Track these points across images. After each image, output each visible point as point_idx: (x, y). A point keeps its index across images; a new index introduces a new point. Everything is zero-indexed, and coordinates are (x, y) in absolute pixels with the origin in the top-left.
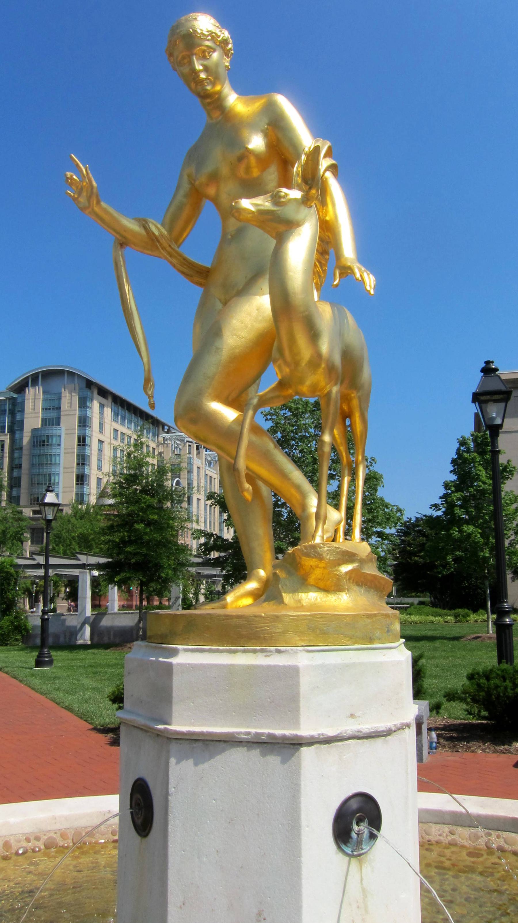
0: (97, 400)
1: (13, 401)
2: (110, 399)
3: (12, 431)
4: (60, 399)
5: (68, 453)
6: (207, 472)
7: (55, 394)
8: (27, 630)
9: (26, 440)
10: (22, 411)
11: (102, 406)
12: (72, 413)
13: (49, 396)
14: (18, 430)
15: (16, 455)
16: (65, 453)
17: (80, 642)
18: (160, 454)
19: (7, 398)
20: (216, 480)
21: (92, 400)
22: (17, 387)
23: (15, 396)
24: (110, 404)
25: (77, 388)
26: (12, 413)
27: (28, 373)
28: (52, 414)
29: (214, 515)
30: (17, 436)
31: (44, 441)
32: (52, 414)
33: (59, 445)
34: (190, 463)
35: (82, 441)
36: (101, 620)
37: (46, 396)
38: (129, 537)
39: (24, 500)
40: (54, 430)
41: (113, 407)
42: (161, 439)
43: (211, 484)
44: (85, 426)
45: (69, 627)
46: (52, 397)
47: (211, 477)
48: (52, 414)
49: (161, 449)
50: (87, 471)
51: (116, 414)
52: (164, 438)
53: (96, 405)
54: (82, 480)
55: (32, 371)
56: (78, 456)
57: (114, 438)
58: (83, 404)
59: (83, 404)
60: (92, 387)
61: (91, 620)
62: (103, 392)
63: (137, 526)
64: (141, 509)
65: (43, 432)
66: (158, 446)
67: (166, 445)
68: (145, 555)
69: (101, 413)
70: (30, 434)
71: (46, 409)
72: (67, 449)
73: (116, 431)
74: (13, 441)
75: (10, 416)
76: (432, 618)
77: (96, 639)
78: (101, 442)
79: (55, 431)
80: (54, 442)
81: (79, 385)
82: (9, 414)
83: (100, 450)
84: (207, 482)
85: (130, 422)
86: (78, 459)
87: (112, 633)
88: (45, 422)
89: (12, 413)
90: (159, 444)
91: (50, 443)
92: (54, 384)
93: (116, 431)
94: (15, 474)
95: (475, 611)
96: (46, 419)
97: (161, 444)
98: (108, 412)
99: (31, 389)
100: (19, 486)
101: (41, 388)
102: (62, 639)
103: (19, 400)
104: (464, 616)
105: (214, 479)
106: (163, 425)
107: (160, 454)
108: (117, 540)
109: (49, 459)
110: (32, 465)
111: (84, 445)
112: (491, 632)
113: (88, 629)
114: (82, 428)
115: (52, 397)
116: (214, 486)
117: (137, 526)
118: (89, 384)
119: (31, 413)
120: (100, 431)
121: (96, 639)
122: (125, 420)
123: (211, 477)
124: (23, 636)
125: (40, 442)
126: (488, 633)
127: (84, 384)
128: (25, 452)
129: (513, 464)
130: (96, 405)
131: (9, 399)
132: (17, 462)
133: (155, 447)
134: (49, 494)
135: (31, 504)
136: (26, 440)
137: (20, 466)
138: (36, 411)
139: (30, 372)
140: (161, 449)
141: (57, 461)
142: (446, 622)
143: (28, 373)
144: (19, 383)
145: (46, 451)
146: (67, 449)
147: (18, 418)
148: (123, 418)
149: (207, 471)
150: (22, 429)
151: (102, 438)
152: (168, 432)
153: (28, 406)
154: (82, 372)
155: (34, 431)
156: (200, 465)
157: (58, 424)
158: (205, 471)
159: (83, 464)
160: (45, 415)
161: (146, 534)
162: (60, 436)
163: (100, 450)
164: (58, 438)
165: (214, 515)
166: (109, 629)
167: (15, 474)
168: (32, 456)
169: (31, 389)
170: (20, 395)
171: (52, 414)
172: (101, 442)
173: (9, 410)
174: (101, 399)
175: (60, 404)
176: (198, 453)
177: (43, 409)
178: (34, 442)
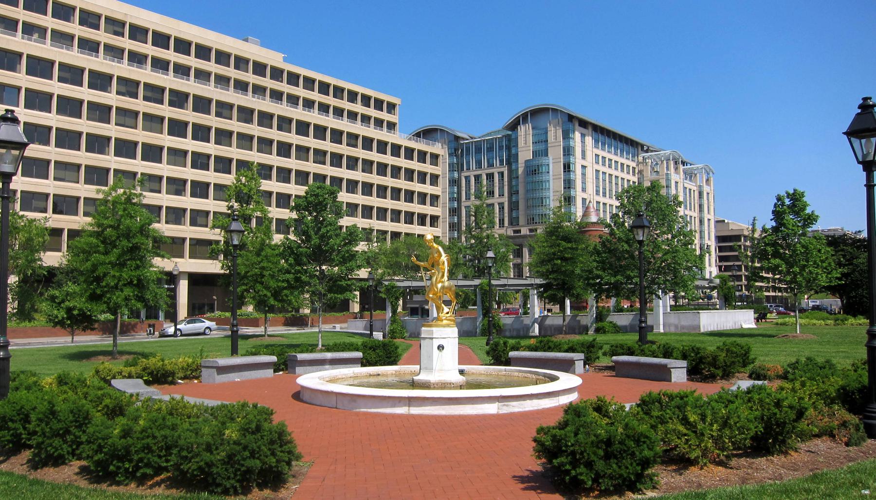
0: (579, 131)
1: (508, 137)
2: (590, 129)
3: (509, 163)
4: (547, 133)
5: (556, 179)
6: (686, 185)
7: (543, 129)
8: (499, 326)
9: (521, 170)
10: (517, 146)
11: (583, 136)
12: (557, 144)
13: (538, 131)
14: (514, 162)
15: (514, 183)
16: (553, 179)
17: (531, 334)
18: (640, 172)
19: (503, 136)
20: (696, 192)
21: (574, 132)
22: (512, 125)
23: (510, 133)
24: (591, 132)
25: (560, 123)
26: (509, 148)
27: (519, 113)
28: (541, 147)
29: (695, 224)
30: (514, 167)
31: (535, 171)
32: (541, 147)
33: (548, 172)
34: (668, 180)
35: (567, 168)
36: (546, 320)
37: (535, 132)
38: (552, 268)
39: (522, 221)
40: (543, 160)
41: (594, 135)
42: (641, 159)
43: (690, 196)
44: (569, 155)
45: (525, 325)
46: (540, 132)
47: (690, 190)
48: (541, 147)
49: (641, 167)
50: (572, 193)
51: (596, 141)
52: (643, 157)
53: (577, 135)
54: (569, 201)
55: (522, 111)
56: (564, 180)
57: (596, 162)
58: (566, 136)
59: (566, 136)
60: (573, 120)
61: (539, 320)
62: (584, 124)
63: (556, 262)
64: (561, 252)
65: (534, 162)
66: (637, 165)
67: (645, 164)
68: (563, 280)
69: (583, 142)
70: (524, 165)
71: (536, 143)
72: (556, 175)
73: (597, 156)
74: (510, 171)
75: (507, 150)
76: (814, 321)
77: (543, 333)
78: (584, 167)
79: (544, 161)
80: (544, 170)
81: (562, 119)
82: (506, 149)
83: (584, 175)
84: (686, 195)
85: (610, 146)
86: (565, 183)
87: (553, 329)
88: (535, 153)
89: (509, 148)
90: (638, 163)
91: (540, 171)
92: (541, 120)
93: (597, 156)
94: (514, 199)
95: (855, 316)
96: (536, 151)
97: (641, 163)
98: (589, 140)
99: (522, 126)
100: (518, 209)
101: (530, 125)
102: (522, 333)
103: (513, 137)
104: (842, 320)
105: (694, 191)
106: (642, 146)
107: (640, 172)
108: (544, 271)
109: (541, 185)
110: (527, 191)
111: (569, 171)
112: (798, 332)
113: (537, 326)
114: (566, 157)
115: (540, 132)
116: (694, 197)
117: (556, 262)
118: (571, 118)
119: (523, 147)
120: (582, 158)
121: (543, 333)
122: (605, 145)
123: (690, 190)
124: (497, 331)
125: (532, 171)
126: (796, 333)
127: (566, 118)
128: (521, 180)
129: (816, 213)
130: (577, 135)
131: (505, 136)
132: (514, 189)
133: (635, 166)
134: (489, 252)
135: (528, 224)
136: (521, 170)
137: (517, 192)
138: (528, 145)
139: (520, 112)
140: (641, 167)
141: (547, 187)
142: (827, 325)
143: (519, 113)
144: (512, 122)
145: (537, 178)
146: (556, 175)
147: (513, 151)
148: (603, 144)
149: (685, 184)
150: (517, 161)
151: (584, 163)
152: (647, 151)
153: (521, 142)
154: (563, 108)
155: (527, 161)
156: (678, 180)
157: (547, 155)
158: (683, 185)
159: (569, 188)
160: (535, 148)
161: (563, 266)
162: (548, 165)
163: (584, 175)
164: (547, 167)
165: (695, 224)
166: (551, 326)
167: (514, 199)
168: (527, 183)
169: (522, 126)
170: (514, 132)
171: (541, 147)
172: (584, 167)
173: (506, 146)
174: (582, 129)
175: (547, 137)
176: (676, 169)
177: (533, 143)
178: (527, 172)
